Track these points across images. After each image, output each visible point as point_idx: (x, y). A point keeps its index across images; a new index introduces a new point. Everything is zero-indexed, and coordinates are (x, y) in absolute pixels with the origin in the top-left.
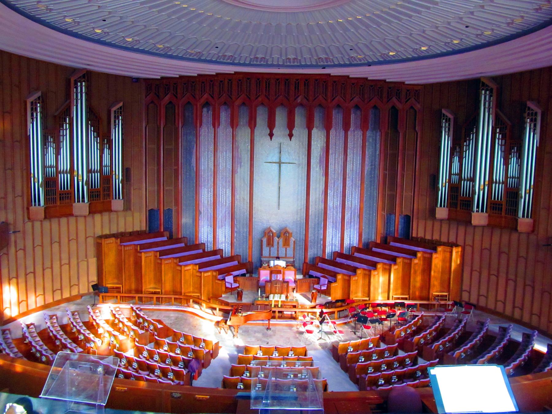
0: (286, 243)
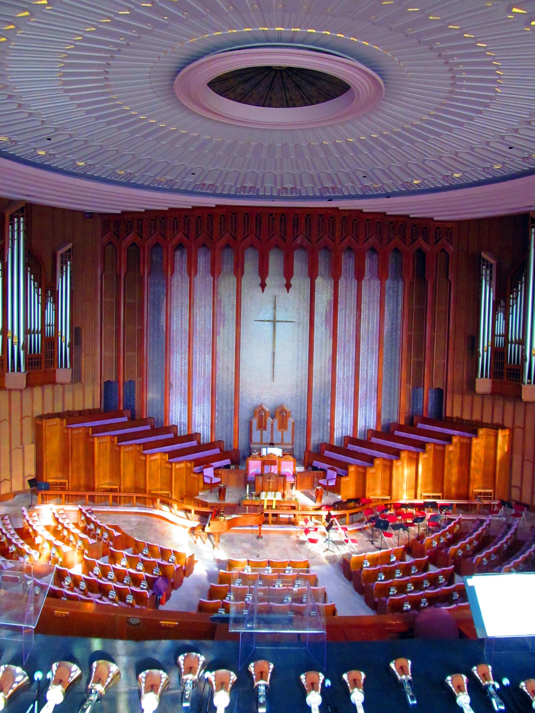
0: (283, 425)
